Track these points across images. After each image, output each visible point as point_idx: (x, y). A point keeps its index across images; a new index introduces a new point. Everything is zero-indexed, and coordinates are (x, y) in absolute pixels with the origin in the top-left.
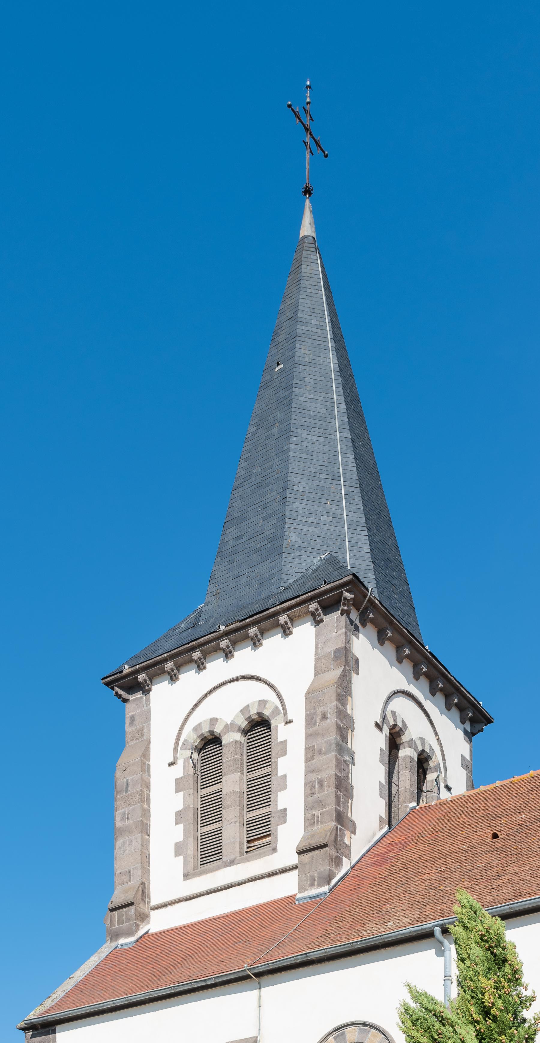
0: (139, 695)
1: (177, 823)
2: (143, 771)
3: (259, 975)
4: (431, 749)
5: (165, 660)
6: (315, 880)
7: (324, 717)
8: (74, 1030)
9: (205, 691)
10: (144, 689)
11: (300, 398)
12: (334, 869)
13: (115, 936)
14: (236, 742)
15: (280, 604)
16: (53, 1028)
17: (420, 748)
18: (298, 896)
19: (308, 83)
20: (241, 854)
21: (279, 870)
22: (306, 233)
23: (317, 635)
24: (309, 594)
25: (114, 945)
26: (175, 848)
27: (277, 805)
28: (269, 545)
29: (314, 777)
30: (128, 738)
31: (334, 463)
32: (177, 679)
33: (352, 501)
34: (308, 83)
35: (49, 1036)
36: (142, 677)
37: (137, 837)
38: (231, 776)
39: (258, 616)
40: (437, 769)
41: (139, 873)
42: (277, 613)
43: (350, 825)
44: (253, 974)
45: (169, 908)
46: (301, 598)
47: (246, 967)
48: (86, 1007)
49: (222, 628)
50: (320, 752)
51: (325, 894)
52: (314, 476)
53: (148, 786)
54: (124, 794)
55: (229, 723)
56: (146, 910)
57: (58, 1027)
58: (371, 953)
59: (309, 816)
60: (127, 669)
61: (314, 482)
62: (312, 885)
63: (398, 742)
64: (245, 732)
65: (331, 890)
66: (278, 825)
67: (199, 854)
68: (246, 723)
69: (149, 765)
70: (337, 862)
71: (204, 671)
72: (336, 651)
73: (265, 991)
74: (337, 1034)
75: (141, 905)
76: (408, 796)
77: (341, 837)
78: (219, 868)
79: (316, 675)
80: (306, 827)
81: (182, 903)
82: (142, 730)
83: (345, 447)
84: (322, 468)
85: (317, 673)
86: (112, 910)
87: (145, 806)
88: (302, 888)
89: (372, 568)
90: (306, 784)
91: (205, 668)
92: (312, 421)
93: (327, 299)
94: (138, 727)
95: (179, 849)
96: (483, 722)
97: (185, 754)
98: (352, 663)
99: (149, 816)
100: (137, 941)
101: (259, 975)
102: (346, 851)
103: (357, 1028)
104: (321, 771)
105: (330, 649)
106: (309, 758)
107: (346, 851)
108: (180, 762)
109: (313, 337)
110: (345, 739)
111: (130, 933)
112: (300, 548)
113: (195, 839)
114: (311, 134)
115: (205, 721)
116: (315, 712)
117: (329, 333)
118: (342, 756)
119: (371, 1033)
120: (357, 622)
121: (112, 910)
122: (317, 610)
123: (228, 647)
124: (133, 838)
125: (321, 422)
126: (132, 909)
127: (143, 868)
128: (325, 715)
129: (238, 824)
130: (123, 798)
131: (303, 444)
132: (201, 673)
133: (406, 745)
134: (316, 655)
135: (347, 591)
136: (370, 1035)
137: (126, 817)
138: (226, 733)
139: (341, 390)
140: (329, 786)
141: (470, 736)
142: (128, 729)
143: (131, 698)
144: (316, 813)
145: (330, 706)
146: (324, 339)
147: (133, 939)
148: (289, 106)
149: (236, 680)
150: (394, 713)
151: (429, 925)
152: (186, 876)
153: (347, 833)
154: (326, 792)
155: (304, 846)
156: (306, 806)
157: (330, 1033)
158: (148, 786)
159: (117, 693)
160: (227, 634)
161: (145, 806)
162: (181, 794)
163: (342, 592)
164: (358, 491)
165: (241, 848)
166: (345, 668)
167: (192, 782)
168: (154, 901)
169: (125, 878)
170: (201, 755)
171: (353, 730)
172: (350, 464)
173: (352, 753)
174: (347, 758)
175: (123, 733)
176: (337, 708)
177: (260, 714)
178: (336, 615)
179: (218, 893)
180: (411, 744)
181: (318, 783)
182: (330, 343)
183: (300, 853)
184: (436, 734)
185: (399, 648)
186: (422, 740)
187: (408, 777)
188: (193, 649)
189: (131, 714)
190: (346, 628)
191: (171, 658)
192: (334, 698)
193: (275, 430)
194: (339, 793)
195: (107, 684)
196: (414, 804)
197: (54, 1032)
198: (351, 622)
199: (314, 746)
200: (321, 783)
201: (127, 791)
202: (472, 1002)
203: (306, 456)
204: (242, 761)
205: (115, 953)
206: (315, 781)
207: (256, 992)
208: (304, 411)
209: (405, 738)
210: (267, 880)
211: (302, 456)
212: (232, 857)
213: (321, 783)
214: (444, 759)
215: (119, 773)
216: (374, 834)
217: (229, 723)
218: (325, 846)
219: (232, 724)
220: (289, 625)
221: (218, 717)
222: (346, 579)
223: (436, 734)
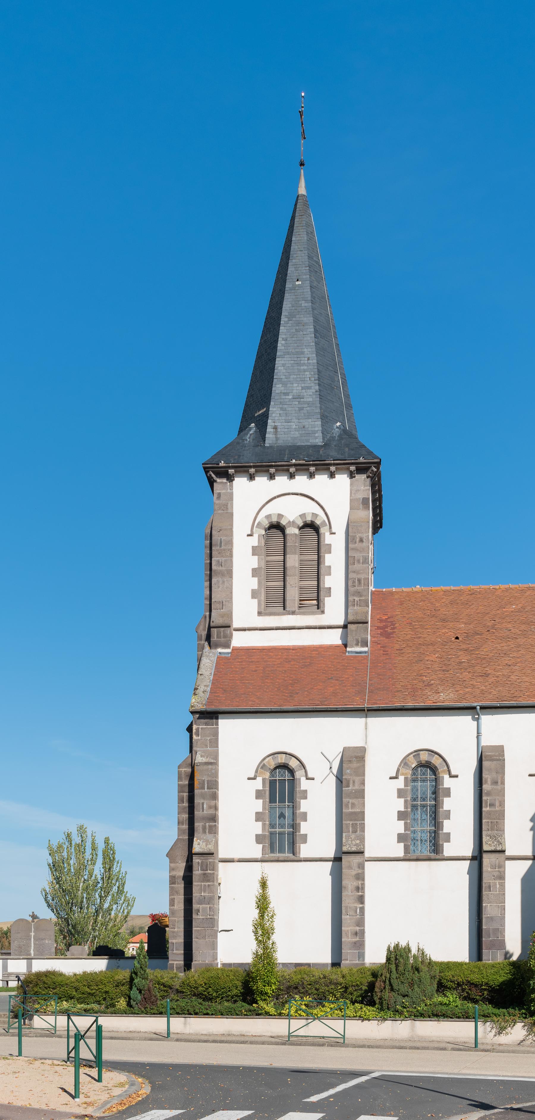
1: (253, 576)
5: (251, 467)
6: (359, 642)
8: (233, 720)
10: (230, 478)
14: (296, 534)
16: (216, 715)
21: (327, 626)
23: (351, 485)
24: (353, 461)
26: (252, 593)
27: (324, 583)
35: (212, 720)
36: (231, 471)
42: (330, 464)
45: (247, 632)
50: (359, 561)
55: (291, 521)
57: (220, 716)
58: (432, 711)
62: (357, 645)
64: (300, 528)
66: (325, 597)
71: (274, 481)
73: (370, 720)
79: (351, 509)
81: (257, 631)
82: (227, 506)
94: (224, 502)
103: (427, 752)
104: (359, 573)
108: (256, 536)
116: (356, 536)
119: (435, 757)
124: (225, 580)
128: (362, 540)
132: (271, 481)
135: (374, 466)
136: (434, 758)
138: (289, 527)
143: (218, 480)
151: (475, 704)
154: (363, 588)
155: (353, 619)
157: (412, 753)
160: (295, 465)
163: (371, 466)
178: (364, 476)
179: (284, 630)
181: (358, 580)
188: (271, 466)
191: (254, 467)
197: (217, 718)
199: (355, 556)
200: (359, 581)
201: (221, 546)
206: (355, 579)
207: (364, 719)
210: (318, 630)
212: (293, 609)
217: (291, 521)
219: (293, 522)
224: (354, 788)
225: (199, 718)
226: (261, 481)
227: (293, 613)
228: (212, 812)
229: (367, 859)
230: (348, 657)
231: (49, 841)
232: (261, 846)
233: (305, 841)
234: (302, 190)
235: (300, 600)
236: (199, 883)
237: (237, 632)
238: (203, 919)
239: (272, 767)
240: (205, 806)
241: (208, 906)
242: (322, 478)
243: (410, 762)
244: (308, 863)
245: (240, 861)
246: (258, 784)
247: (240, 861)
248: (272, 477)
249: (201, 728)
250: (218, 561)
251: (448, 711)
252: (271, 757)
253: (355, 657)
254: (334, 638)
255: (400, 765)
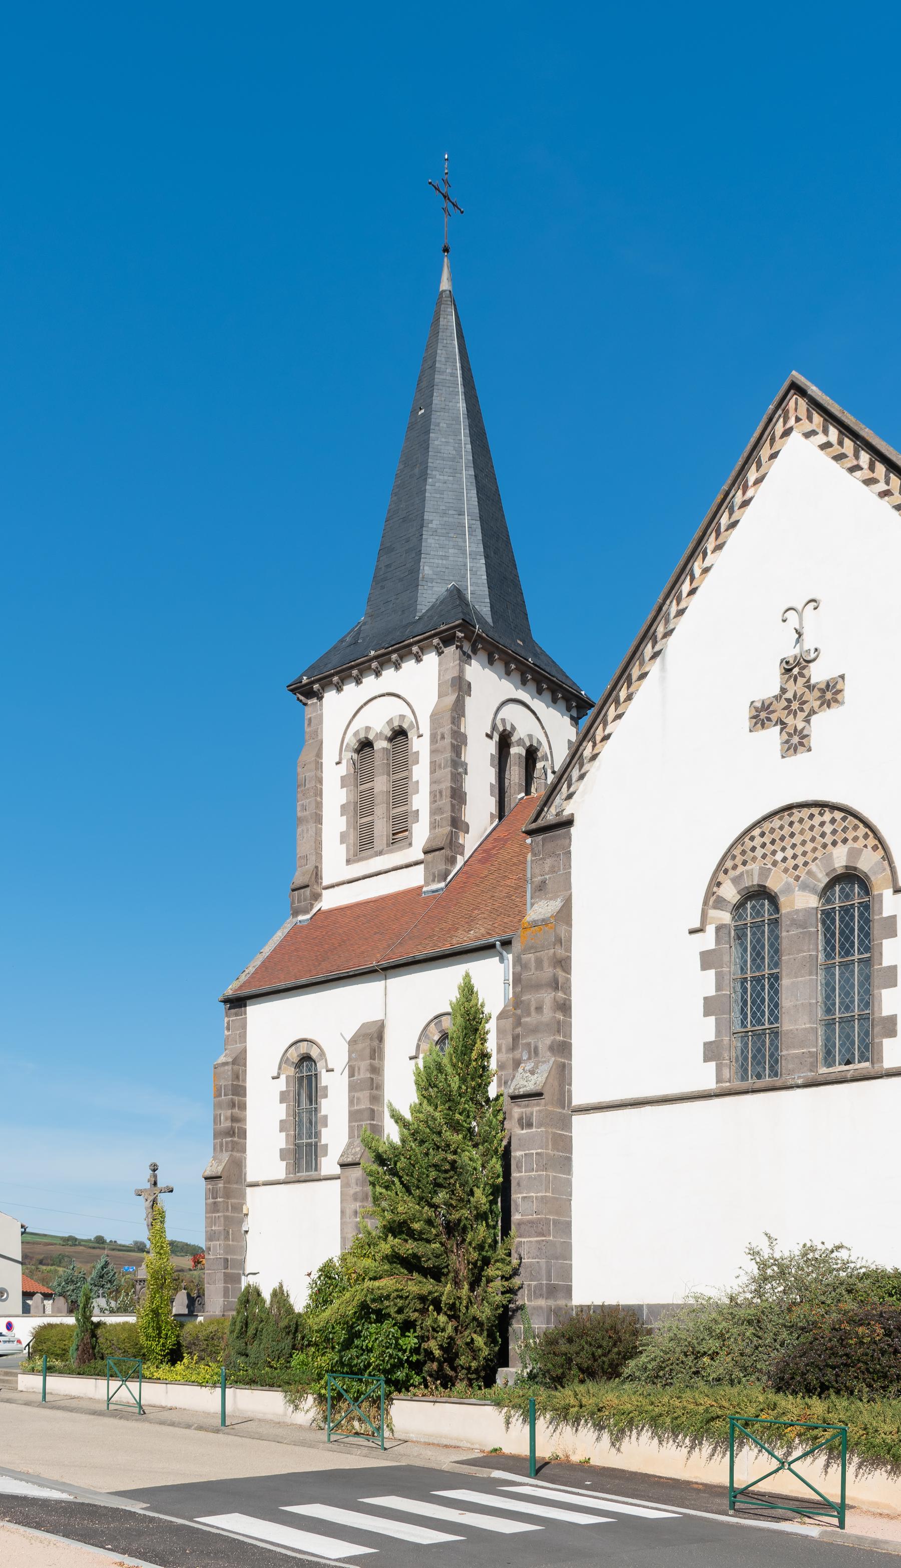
0: (315, 700)
1: (342, 815)
2: (317, 769)
3: (385, 969)
4: (539, 742)
5: (333, 675)
7: (443, 737)
9: (362, 703)
11: (436, 443)
12: (449, 868)
13: (296, 913)
14: (383, 748)
15: (413, 638)
17: (528, 744)
18: (425, 889)
19: (446, 157)
20: (388, 845)
22: (444, 288)
23: (440, 664)
25: (295, 920)
28: (410, 576)
29: (437, 787)
30: (307, 737)
31: (461, 500)
32: (342, 690)
33: (474, 533)
34: (446, 157)
36: (316, 687)
37: (312, 826)
38: (380, 778)
39: (397, 646)
40: (545, 758)
41: (314, 858)
43: (464, 827)
44: (381, 969)
45: (336, 888)
46: (427, 634)
47: (374, 963)
48: (266, 988)
49: (373, 653)
51: (442, 889)
52: (445, 513)
53: (320, 781)
54: (303, 788)
56: (319, 890)
57: (248, 1002)
59: (433, 821)
60: (305, 680)
61: (445, 519)
62: (433, 881)
63: (509, 742)
64: (390, 740)
65: (446, 886)
67: (359, 841)
68: (391, 733)
69: (322, 763)
70: (452, 861)
72: (453, 679)
74: (436, 1021)
75: (315, 887)
76: (517, 789)
77: (456, 839)
78: (371, 857)
80: (430, 829)
83: (469, 484)
84: (451, 505)
85: (439, 697)
86: (293, 890)
87: (319, 799)
88: (427, 883)
89: (487, 593)
90: (431, 793)
91: (361, 682)
92: (445, 462)
93: (459, 349)
95: (343, 838)
96: (586, 708)
97: (348, 755)
98: (465, 687)
99: (322, 807)
100: (311, 918)
101: (385, 969)
102: (461, 850)
105: (449, 676)
106: (433, 771)
107: (461, 849)
108: (344, 762)
109: (447, 385)
110: (459, 754)
111: (306, 912)
112: (432, 580)
113: (355, 829)
114: (449, 199)
115: (362, 728)
117: (460, 379)
118: (457, 770)
120: (470, 652)
121: (293, 890)
122: (438, 644)
123: (377, 668)
125: (451, 463)
126: (308, 891)
127: (317, 853)
129: (385, 820)
130: (302, 791)
131: (437, 484)
133: (515, 744)
134: (439, 681)
135: (459, 631)
137: (304, 808)
138: (376, 741)
139: (468, 431)
140: (446, 796)
141: (575, 720)
142: (307, 730)
143: (310, 702)
144: (438, 818)
145: (447, 728)
146: (455, 386)
147: (308, 916)
148: (430, 183)
149: (383, 695)
150: (503, 720)
152: (348, 862)
153: (461, 834)
156: (430, 812)
157: (432, 1021)
158: (321, 782)
159: (298, 699)
160: (376, 658)
161: (319, 799)
162: (345, 789)
164: (479, 523)
165: (387, 840)
166: (459, 694)
167: (352, 780)
168: (326, 882)
169: (303, 861)
170: (360, 756)
171: (466, 745)
172: (473, 499)
173: (465, 765)
174: (461, 770)
175: (303, 732)
176: (452, 730)
177: (400, 726)
180: (520, 742)
182: (460, 389)
183: (425, 853)
184: (543, 728)
185: (507, 665)
186: (530, 737)
187: (517, 772)
188: (352, 667)
189: (309, 716)
190: (460, 660)
192: (449, 722)
193: (417, 470)
194: (454, 802)
195: (292, 690)
196: (523, 794)
197: (245, 1006)
198: (464, 653)
200: (441, 792)
201: (305, 786)
202: (455, 1055)
203: (438, 496)
204: (388, 764)
205: (296, 930)
207: (383, 982)
208: (439, 454)
209: (514, 739)
210: (405, 869)
211: (435, 495)
212: (381, 848)
213: (441, 792)
214: (550, 748)
215: (299, 770)
216: (486, 830)
218: (442, 849)
220: (420, 654)
221: (371, 726)
222: (457, 622)
223: (543, 728)
224: (359, 1077)
225: (230, 1009)
226: (350, 688)
227: (381, 853)
228: (501, 1041)
229: (339, 1178)
230: (425, 898)
231: (154, 1168)
232: (285, 1163)
233: (892, 1033)
234: (445, 285)
235: (394, 834)
236: (210, 1215)
237: (327, 890)
238: (214, 1259)
239: (296, 1060)
240: (222, 1118)
241: (218, 1243)
242: (389, 673)
243: (431, 1033)
244: (329, 1182)
245: (266, 1184)
246: (282, 1084)
247: (266, 1184)
248: (358, 682)
249: (232, 1021)
250: (303, 805)
251: (452, 958)
252: (293, 1048)
253: (434, 897)
254: (415, 878)
255: (419, 1040)
